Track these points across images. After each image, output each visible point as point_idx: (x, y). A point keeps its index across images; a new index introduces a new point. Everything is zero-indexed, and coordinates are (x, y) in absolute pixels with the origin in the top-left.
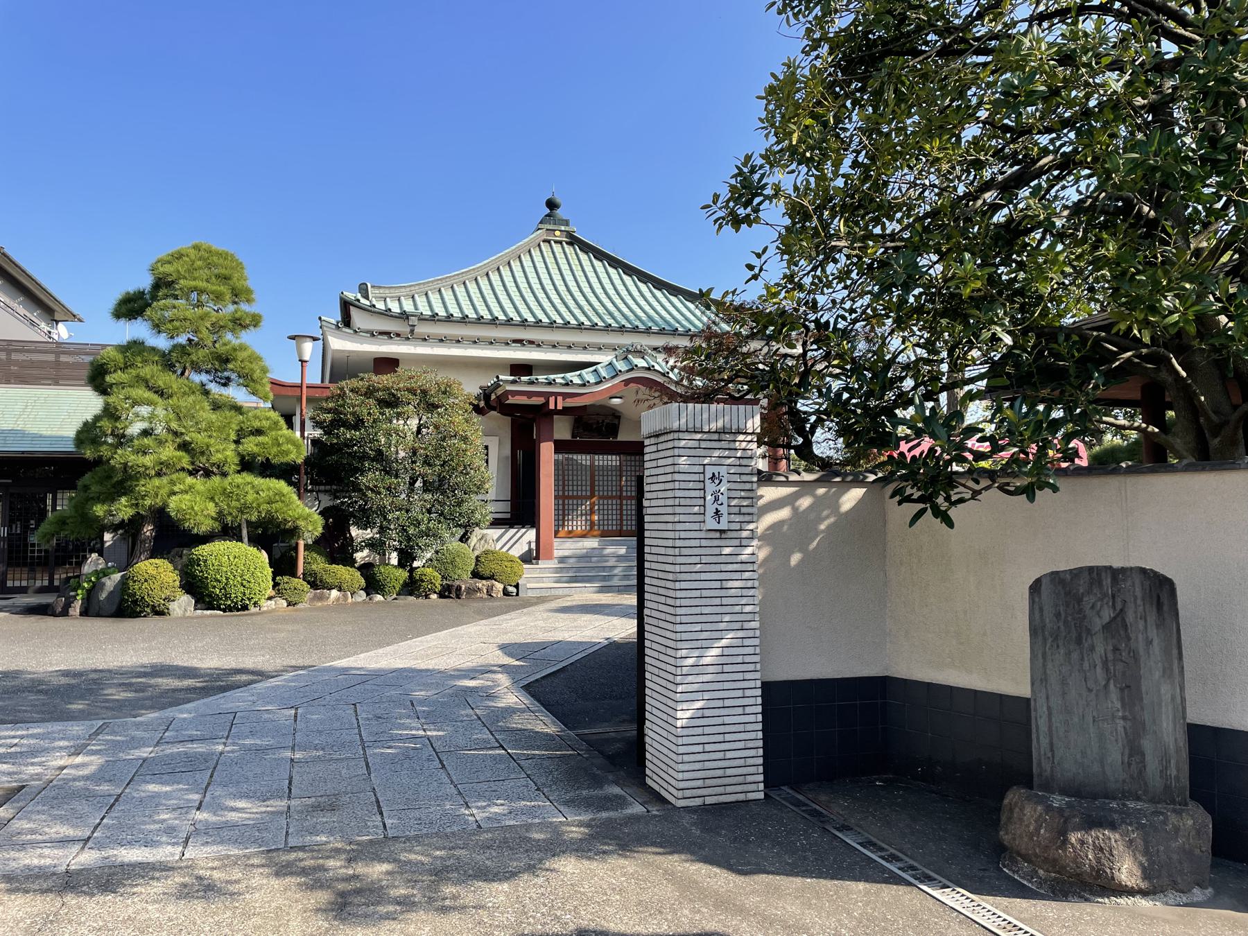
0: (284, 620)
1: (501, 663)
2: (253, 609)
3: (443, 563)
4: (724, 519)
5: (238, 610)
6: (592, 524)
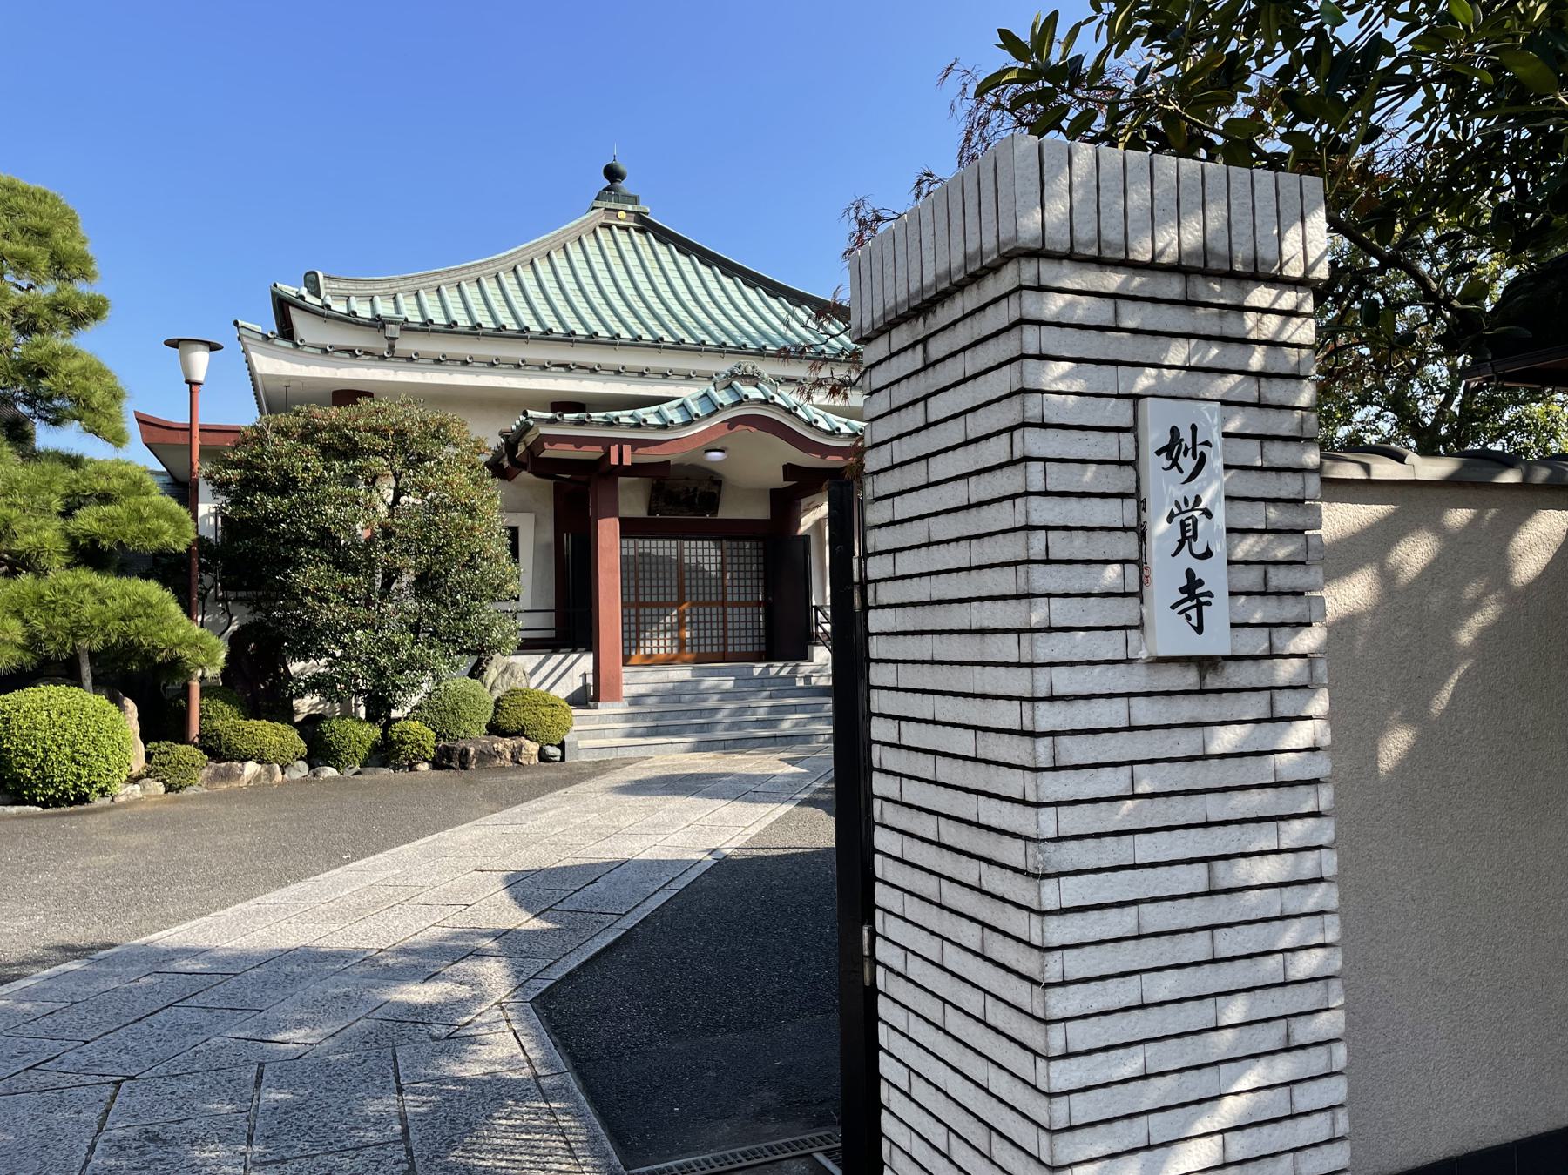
0: (152, 822)
1: (502, 925)
2: (99, 802)
3: (438, 712)
4: (1218, 613)
5: (71, 804)
6: (682, 644)
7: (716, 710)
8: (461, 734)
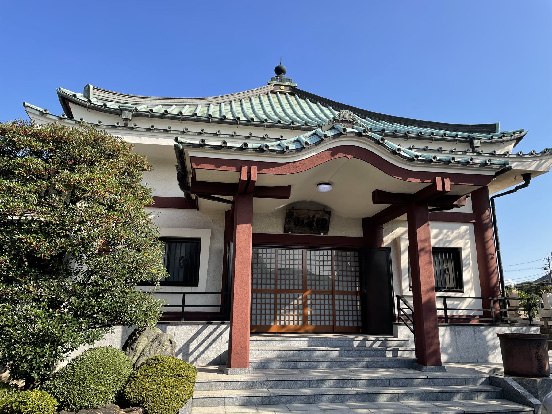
6: (305, 317)
7: (322, 381)
8: (86, 404)
